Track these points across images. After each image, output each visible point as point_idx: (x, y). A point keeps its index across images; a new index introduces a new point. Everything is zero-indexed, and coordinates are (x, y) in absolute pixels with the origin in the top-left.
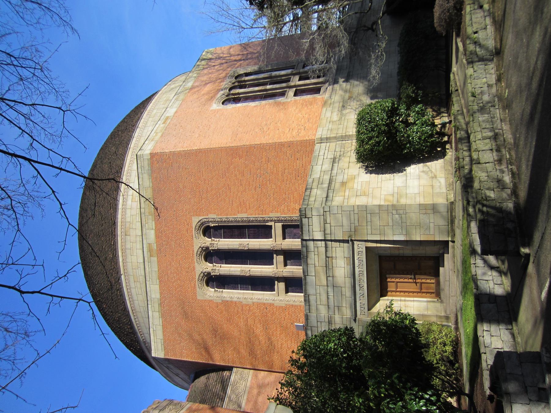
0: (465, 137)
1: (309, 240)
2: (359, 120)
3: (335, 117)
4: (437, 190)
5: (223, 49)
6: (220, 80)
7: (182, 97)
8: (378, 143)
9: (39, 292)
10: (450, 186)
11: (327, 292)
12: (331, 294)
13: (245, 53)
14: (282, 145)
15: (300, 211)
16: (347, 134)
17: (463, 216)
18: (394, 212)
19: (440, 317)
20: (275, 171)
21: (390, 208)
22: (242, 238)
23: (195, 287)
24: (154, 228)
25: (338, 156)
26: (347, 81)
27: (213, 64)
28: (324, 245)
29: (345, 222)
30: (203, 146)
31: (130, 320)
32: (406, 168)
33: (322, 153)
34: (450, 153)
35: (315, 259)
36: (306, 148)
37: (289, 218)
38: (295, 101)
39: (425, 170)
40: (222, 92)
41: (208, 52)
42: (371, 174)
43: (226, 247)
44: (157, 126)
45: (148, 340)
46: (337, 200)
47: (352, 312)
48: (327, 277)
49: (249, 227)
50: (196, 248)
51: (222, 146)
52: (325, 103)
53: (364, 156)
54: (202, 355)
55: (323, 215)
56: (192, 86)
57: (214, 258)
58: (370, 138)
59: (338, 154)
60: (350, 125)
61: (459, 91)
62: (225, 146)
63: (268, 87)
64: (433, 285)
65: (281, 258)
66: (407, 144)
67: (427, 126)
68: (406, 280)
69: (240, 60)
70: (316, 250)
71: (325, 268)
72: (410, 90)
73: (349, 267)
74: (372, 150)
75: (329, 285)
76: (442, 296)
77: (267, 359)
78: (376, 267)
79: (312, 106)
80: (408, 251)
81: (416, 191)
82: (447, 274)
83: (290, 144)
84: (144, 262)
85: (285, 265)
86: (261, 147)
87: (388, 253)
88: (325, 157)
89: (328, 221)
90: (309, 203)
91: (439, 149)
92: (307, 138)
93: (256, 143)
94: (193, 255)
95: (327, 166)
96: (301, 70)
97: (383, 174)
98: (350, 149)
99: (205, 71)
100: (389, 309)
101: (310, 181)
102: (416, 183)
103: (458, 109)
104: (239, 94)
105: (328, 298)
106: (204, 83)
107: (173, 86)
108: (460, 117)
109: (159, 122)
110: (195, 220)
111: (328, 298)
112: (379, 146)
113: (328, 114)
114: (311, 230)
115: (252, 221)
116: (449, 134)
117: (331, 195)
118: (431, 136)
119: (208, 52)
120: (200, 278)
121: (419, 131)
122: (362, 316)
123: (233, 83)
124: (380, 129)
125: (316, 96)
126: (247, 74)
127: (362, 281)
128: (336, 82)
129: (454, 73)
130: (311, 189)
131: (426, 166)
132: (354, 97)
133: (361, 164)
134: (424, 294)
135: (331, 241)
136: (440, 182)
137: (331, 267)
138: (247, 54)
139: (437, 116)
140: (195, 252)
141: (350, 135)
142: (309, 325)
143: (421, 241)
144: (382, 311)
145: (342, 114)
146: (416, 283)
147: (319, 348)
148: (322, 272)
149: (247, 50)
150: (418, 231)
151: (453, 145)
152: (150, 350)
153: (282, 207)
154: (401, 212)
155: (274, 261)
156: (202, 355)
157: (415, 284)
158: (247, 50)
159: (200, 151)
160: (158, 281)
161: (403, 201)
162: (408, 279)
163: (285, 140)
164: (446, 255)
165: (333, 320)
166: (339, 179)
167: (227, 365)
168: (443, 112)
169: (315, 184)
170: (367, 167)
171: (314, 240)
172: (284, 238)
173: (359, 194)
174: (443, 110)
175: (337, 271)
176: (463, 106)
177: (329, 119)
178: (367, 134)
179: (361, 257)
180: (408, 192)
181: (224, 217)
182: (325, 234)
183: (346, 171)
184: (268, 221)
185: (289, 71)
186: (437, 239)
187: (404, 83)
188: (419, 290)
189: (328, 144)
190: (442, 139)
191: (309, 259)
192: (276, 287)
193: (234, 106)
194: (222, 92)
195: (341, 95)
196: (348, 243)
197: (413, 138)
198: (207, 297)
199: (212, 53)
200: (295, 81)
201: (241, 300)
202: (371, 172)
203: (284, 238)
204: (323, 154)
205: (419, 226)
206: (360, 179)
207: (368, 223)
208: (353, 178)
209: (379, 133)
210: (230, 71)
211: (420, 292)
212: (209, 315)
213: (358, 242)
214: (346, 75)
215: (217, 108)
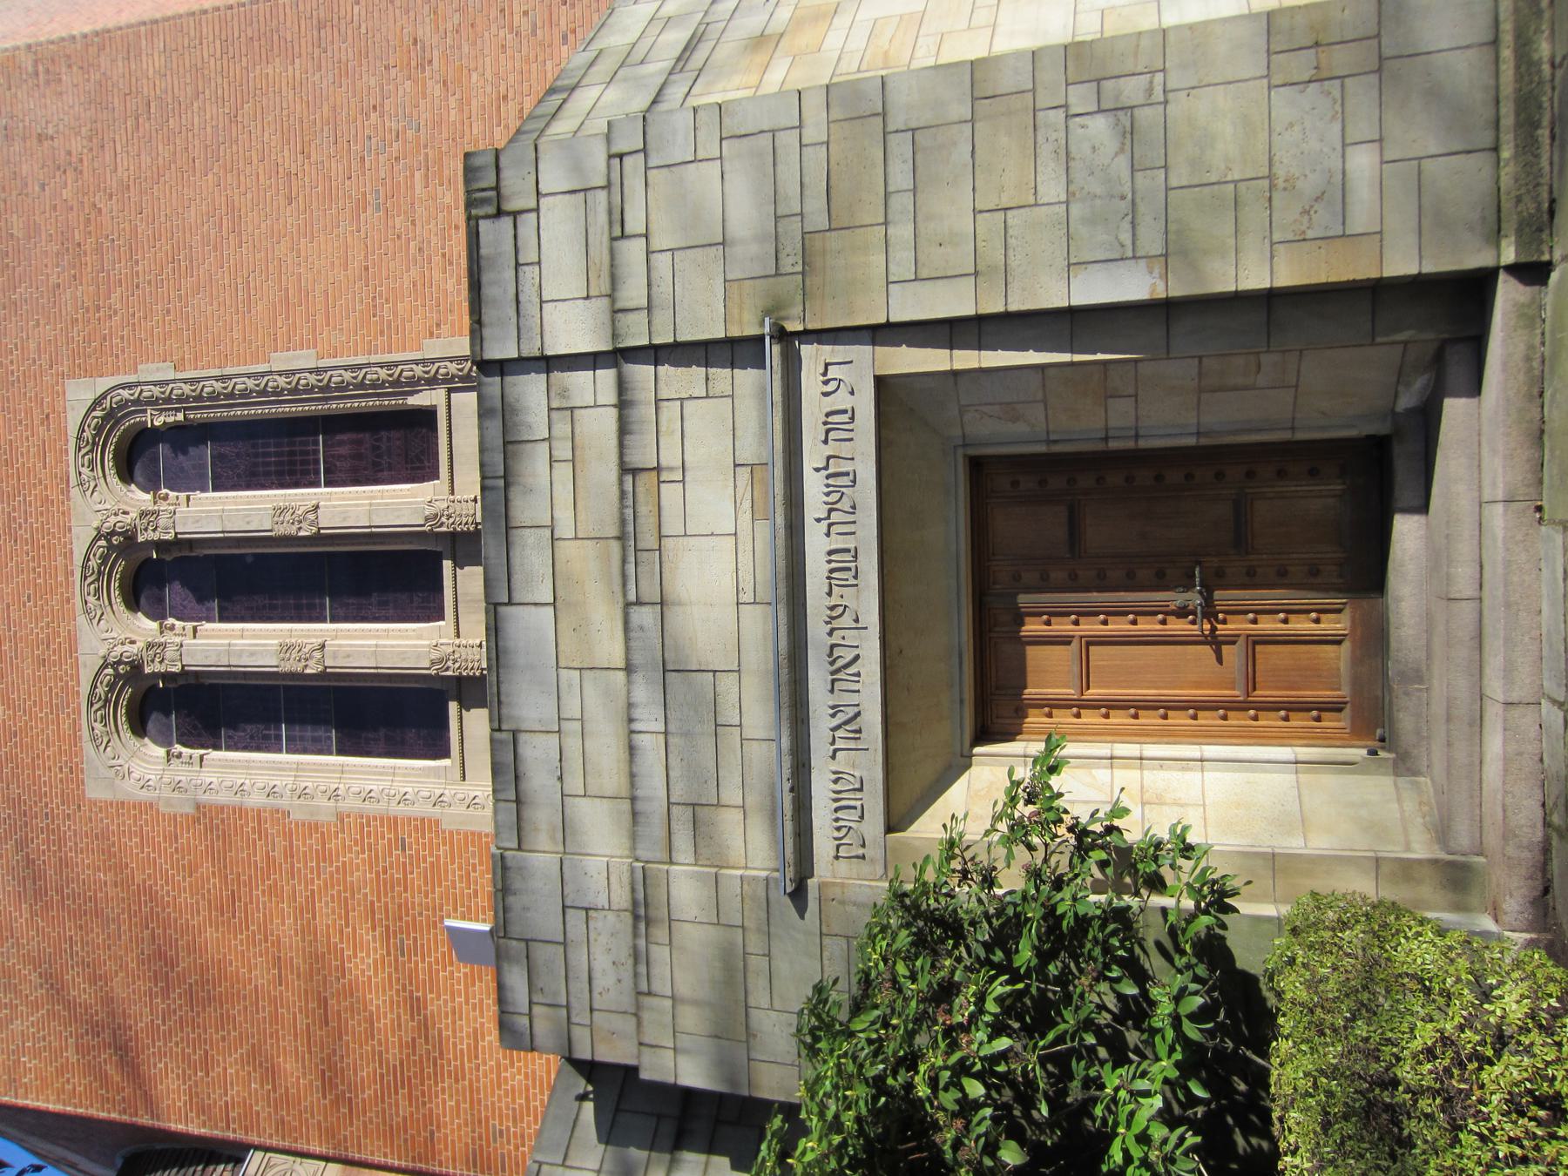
1: (524, 364)
12: (650, 721)
18: (1080, 98)
19: (1406, 869)
22: (297, 485)
23: (75, 739)
28: (608, 395)
29: (745, 214)
47: (778, 842)
48: (628, 605)
49: (332, 424)
54: (104, 1080)
57: (174, 592)
64: (1341, 657)
68: (1148, 626)
70: (562, 428)
71: (615, 546)
73: (763, 529)
75: (637, 659)
76: (1405, 722)
77: (404, 1108)
78: (947, 530)
87: (1022, 433)
89: (635, 223)
94: (69, 573)
100: (1024, 810)
105: (632, 750)
110: (80, 395)
111: (632, 750)
120: (101, 690)
122: (842, 865)
127: (847, 621)
134: (1269, 721)
135: (656, 354)
137: (648, 540)
142: (515, 930)
143: (1270, 298)
144: (973, 831)
146: (1216, 642)
148: (590, 566)
154: (1131, 90)
156: (104, 1080)
157: (1207, 650)
159: (102, 39)
162: (1162, 615)
164: (1454, 409)
165: (659, 895)
167: (217, 1133)
171: (549, 364)
175: (687, 566)
179: (845, 449)
181: (206, 372)
184: (414, 384)
188: (1237, 693)
191: (514, 493)
198: (130, 790)
201: (284, 803)
207: (895, 201)
211: (1241, 707)
213: (828, 352)
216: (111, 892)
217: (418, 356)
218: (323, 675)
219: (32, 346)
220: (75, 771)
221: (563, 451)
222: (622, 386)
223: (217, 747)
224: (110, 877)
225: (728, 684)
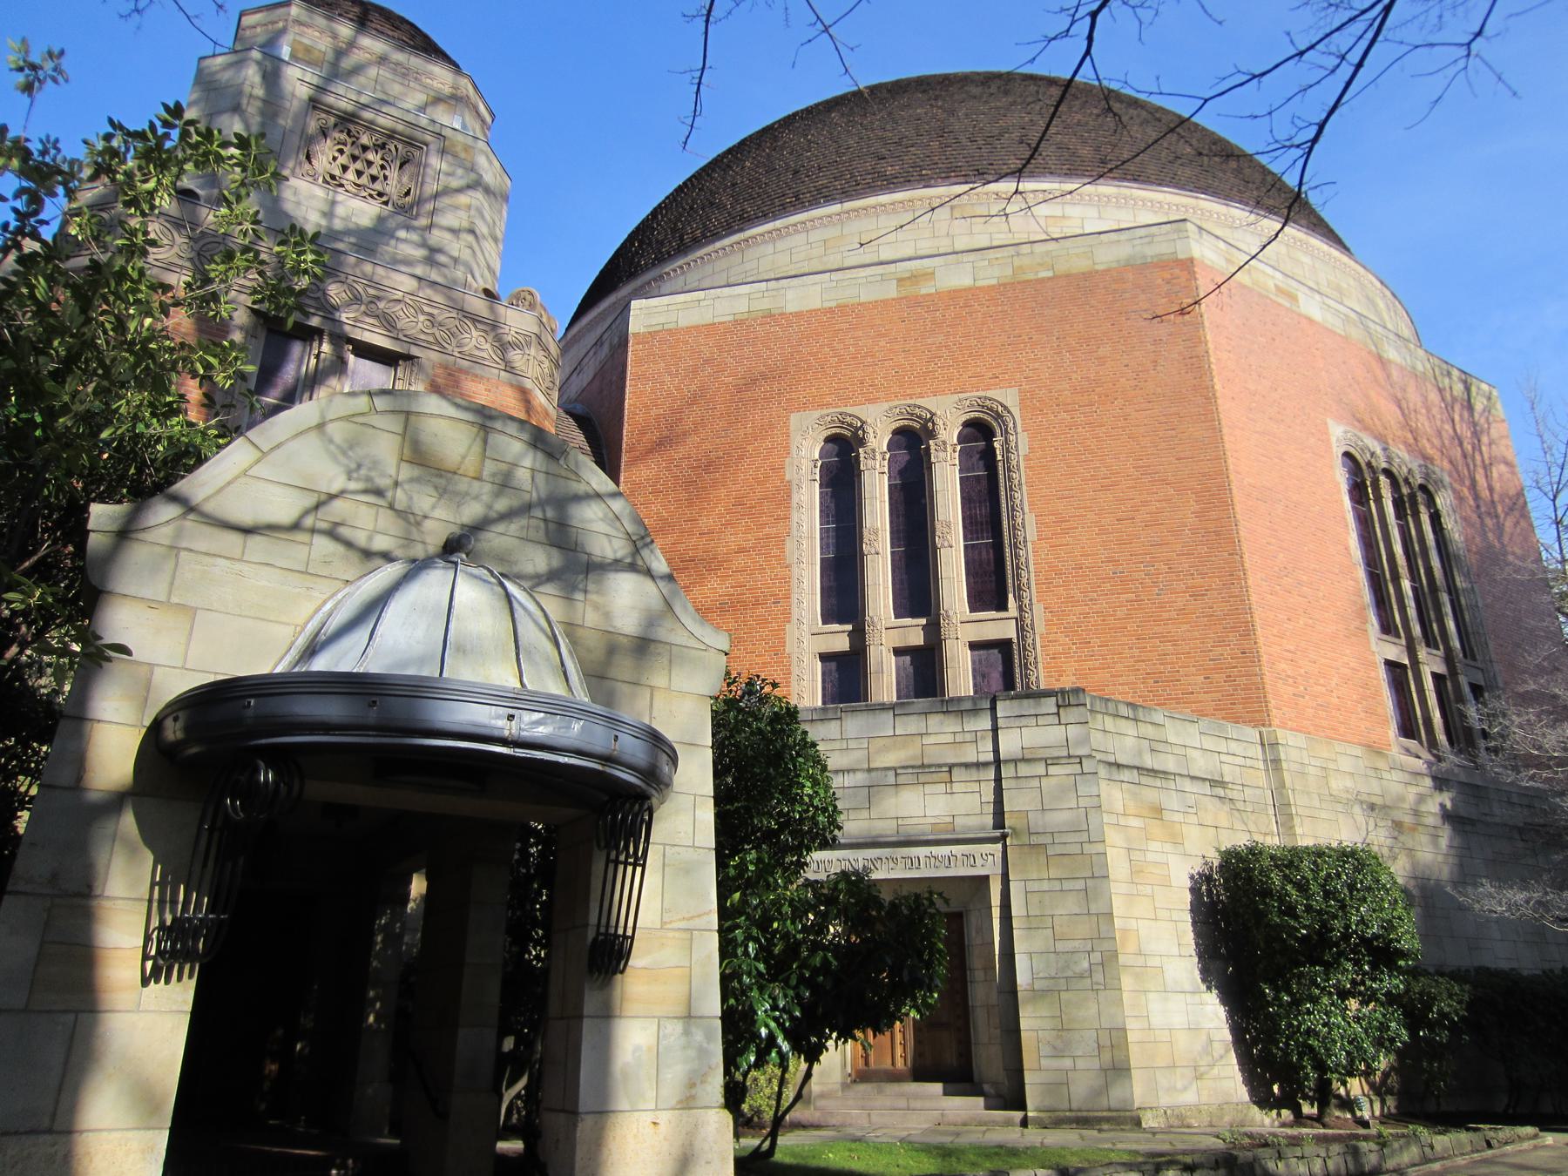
0: (1362, 1165)
1: (994, 719)
2: (1353, 853)
3: (1338, 784)
4: (1163, 1079)
5: (1504, 442)
6: (1412, 441)
7: (1356, 333)
8: (1291, 911)
9: (1088, 52)
10: (1178, 1122)
11: (854, 771)
13: (1500, 509)
14: (1247, 631)
15: (1077, 691)
16: (1297, 821)
17: (1136, 1152)
18: (1096, 958)
20: (1165, 615)
21: (1106, 946)
23: (821, 406)
24: (979, 284)
25: (1230, 794)
26: (1447, 816)
27: (1457, 418)
28: (983, 758)
29: (1058, 819)
30: (1224, 405)
31: (717, 236)
32: (1215, 992)
33: (1234, 747)
34: (1267, 1121)
35: (940, 735)
36: (1240, 699)
37: (1031, 659)
38: (1373, 665)
39: (1216, 1045)
40: (1379, 451)
41: (1489, 399)
42: (1192, 890)
43: (938, 484)
44: (1269, 270)
45: (666, 288)
46: (1114, 795)
48: (895, 769)
50: (930, 403)
51: (1230, 461)
52: (1375, 750)
53: (1245, 870)
55: (1069, 756)
56: (1389, 361)
58: (1302, 887)
59: (1234, 795)
60: (1325, 827)
61: (1490, 1152)
62: (1231, 467)
63: (1406, 585)
64: (887, 1065)
65: (917, 638)
66: (1290, 993)
67: (1348, 1053)
69: (1476, 497)
72: (1449, 1004)
74: (1267, 893)
75: (874, 774)
79: (1363, 715)
80: (981, 994)
81: (1156, 1020)
82: (928, 1104)
83: (1249, 655)
84: (882, 263)
85: (898, 652)
86: (1234, 574)
87: (973, 937)
88: (1224, 758)
89: (1053, 770)
90: (1099, 716)
91: (1276, 1088)
92: (1273, 703)
93: (1246, 556)
94: (911, 396)
95: (1201, 764)
96: (1463, 681)
97: (1194, 923)
98: (1253, 828)
99: (1434, 396)
101: (1158, 717)
102: (1178, 1020)
103: (1438, 1147)
104: (1379, 499)
106: (1399, 395)
107: (1381, 305)
108: (1413, 1152)
109: (1278, 275)
110: (1008, 397)
112: (1281, 913)
113: (1345, 764)
114: (1024, 721)
115: (1017, 556)
116: (1327, 1120)
117: (1126, 775)
118: (1321, 1067)
119: (1489, 399)
120: (848, 419)
121: (1331, 1030)
123: (1406, 481)
124: (1335, 917)
125: (1392, 729)
126: (1436, 518)
128: (1440, 783)
129: (1536, 1136)
130: (1136, 720)
131: (1227, 1051)
132: (1402, 838)
133: (1216, 864)
135: (998, 780)
136: (1185, 1089)
137: (922, 778)
138: (1497, 517)
139: (1372, 1086)
140: (919, 402)
141: (1292, 827)
143: (1018, 1031)
145: (1348, 803)
147: (798, 755)
149: (1507, 514)
150: (1047, 1024)
151: (1289, 1131)
152: (641, 293)
153: (1062, 639)
154: (1098, 977)
155: (908, 621)
156: (642, 433)
158: (1507, 514)
159: (1209, 398)
160: (833, 304)
161: (1127, 982)
163: (1261, 641)
164: (980, 1101)
166: (1171, 801)
168: (1383, 1102)
169: (1149, 731)
170: (1208, 879)
171: (995, 730)
172: (973, 646)
173: (1136, 855)
174: (1391, 1102)
176: (1447, 1163)
177: (1332, 766)
178: (1315, 879)
179: (959, 863)
180: (1151, 996)
181: (1021, 476)
182: (1015, 761)
183: (1193, 819)
184: (1019, 598)
185: (1456, 643)
186: (1029, 1078)
187: (1467, 987)
189: (1261, 765)
190: (1305, 1097)
191: (941, 716)
192: (836, 627)
193: (1344, 487)
194: (1379, 451)
195: (1402, 799)
196: (996, 827)
197: (1309, 1013)
198: (796, 439)
199: (1487, 410)
200: (1431, 664)
202: (1195, 891)
203: (973, 646)
204: (1231, 751)
205: (1063, 1029)
206: (1173, 860)
207: (1057, 883)
208: (1176, 840)
209: (1320, 912)
210: (1442, 469)
212: (750, 448)
214: (1463, 813)
215: (1334, 439)
216: (741, 432)
217: (1034, 601)
218: (862, 555)
219: (1037, 365)
220: (804, 407)
221: (959, 738)
222: (986, 764)
223: (821, 486)
224: (749, 430)
225: (865, 814)
